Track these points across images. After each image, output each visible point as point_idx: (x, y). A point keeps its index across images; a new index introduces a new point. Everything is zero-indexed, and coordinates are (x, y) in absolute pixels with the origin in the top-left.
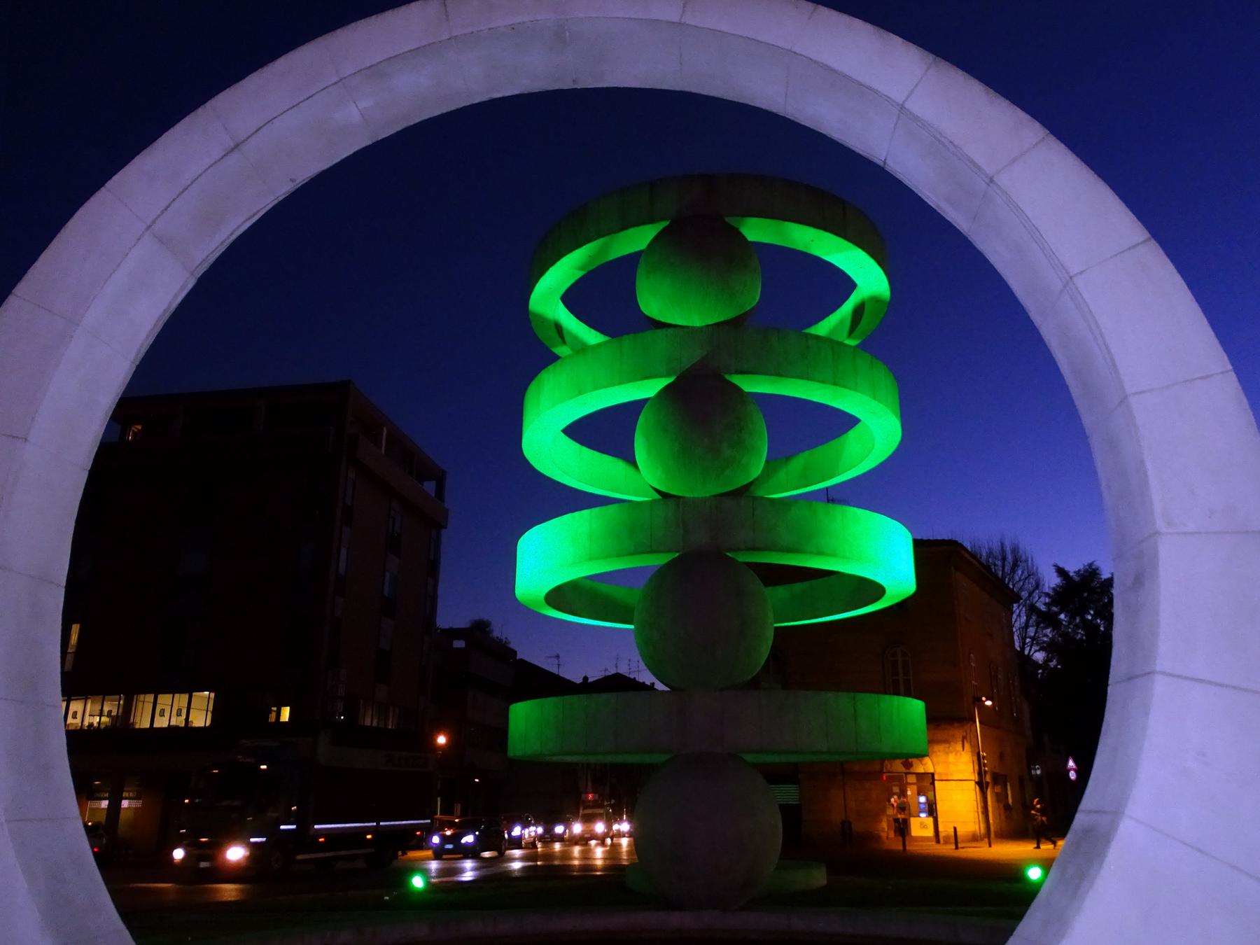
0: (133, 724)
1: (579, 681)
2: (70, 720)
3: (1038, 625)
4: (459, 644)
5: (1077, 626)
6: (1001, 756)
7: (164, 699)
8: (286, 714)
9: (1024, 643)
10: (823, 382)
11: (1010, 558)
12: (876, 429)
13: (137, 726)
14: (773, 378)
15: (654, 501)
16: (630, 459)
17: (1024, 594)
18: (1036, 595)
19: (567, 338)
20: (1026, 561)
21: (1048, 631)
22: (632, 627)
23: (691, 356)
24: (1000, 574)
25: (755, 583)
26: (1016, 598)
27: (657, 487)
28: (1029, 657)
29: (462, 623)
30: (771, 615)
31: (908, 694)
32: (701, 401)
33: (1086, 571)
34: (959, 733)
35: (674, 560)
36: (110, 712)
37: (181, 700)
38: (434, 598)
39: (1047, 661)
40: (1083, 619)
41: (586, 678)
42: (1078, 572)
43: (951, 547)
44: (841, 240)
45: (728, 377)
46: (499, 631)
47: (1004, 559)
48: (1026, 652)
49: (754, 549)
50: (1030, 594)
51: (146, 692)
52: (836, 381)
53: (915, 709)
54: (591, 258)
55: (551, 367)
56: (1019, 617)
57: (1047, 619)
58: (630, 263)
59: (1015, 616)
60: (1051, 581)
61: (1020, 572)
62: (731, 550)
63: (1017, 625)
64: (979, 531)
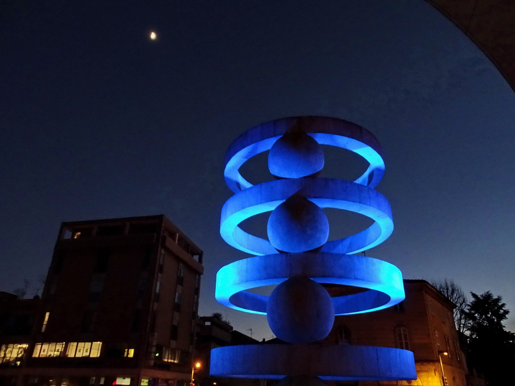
0: (67, 355)
1: (261, 340)
2: (42, 353)
3: (465, 318)
4: (208, 323)
5: (484, 319)
6: (454, 379)
7: (81, 344)
8: (131, 353)
9: (460, 327)
10: (354, 202)
11: (450, 289)
12: (384, 225)
13: (69, 356)
14: (330, 200)
15: (275, 255)
16: (266, 238)
17: (458, 305)
18: (463, 305)
19: (242, 189)
20: (458, 290)
21: (471, 321)
22: (266, 314)
23: (292, 191)
24: (446, 296)
25: (325, 293)
26: (455, 306)
27: (277, 248)
28: (463, 333)
29: (209, 314)
30: (333, 310)
31: (407, 349)
32: (297, 211)
33: (486, 295)
34: (433, 368)
35: (286, 281)
36: (58, 350)
37: (88, 345)
38: (197, 304)
39: (471, 335)
40: (486, 317)
41: (264, 340)
42: (482, 296)
43: (423, 283)
44: (362, 143)
45: (309, 199)
46: (224, 318)
47: (447, 289)
48: (461, 331)
49: (324, 276)
50: (461, 304)
51: (74, 342)
52: (361, 202)
53: (409, 355)
54: (250, 153)
55: (231, 198)
56: (457, 315)
57: (469, 316)
58: (265, 154)
59: (454, 315)
60: (470, 299)
61: (455, 295)
62: (312, 277)
63: (456, 318)
64: (436, 277)
